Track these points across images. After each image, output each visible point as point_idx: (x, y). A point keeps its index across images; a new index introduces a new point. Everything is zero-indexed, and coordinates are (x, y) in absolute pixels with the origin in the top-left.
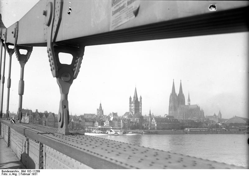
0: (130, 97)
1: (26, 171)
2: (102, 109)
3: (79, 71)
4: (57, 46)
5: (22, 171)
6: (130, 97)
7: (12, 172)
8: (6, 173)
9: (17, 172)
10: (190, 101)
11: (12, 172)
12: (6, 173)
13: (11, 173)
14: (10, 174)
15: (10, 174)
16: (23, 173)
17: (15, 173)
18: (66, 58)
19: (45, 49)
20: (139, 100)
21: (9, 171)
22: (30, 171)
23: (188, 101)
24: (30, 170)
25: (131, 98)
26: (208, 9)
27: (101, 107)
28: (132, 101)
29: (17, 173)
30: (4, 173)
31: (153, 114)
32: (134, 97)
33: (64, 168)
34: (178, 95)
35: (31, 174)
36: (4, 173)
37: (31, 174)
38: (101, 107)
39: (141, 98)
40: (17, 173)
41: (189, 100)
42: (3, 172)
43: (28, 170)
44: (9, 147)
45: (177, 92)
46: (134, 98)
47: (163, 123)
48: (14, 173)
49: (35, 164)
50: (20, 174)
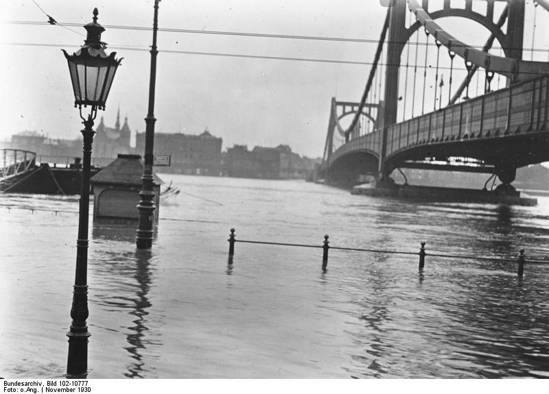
1: (58, 383)
4: (509, 19)
5: (48, 383)
7: (27, 384)
8: (13, 387)
9: (37, 385)
11: (27, 384)
12: (13, 387)
13: (25, 388)
14: (22, 390)
15: (22, 390)
16: (8, 387)
17: (33, 387)
18: (490, 74)
19: (91, 21)
21: (19, 384)
22: (66, 383)
24: (77, 380)
26: (158, 19)
29: (39, 388)
30: (10, 387)
33: (525, 374)
35: (77, 390)
36: (10, 387)
37: (77, 390)
40: (39, 388)
42: (7, 386)
43: (74, 380)
48: (31, 387)
50: (44, 389)
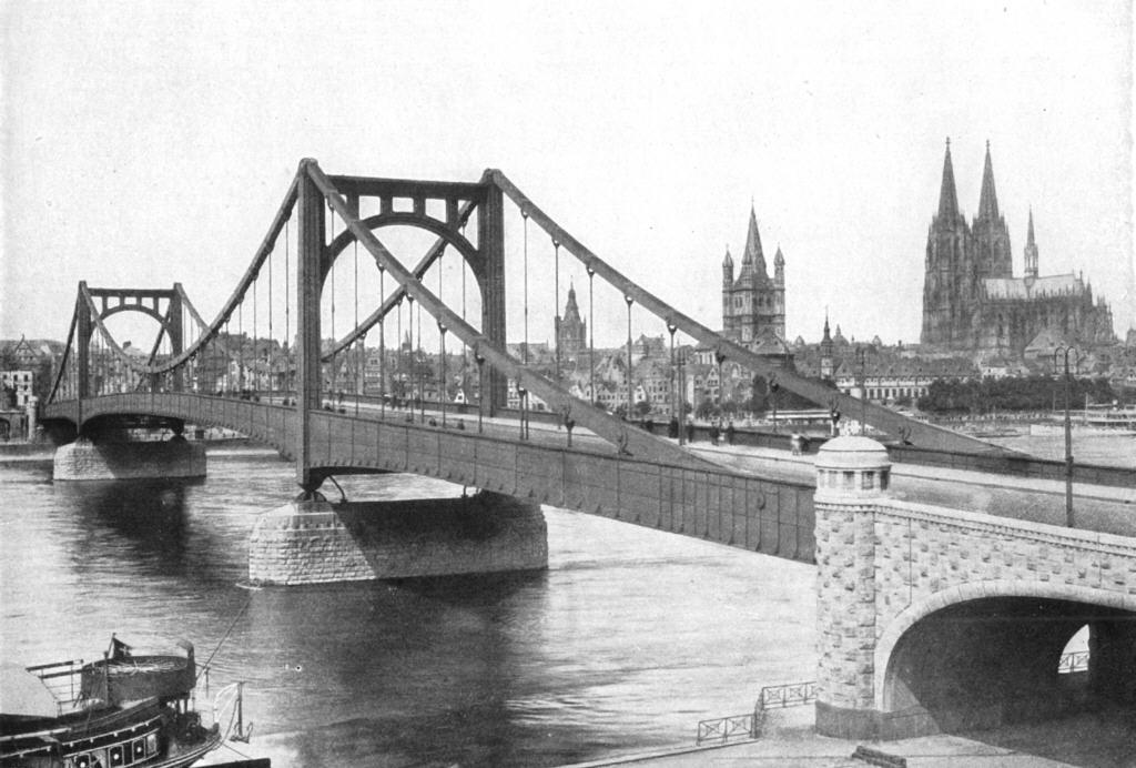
0: (779, 251)
2: (578, 317)
3: (243, 297)
6: (779, 251)
10: (1035, 254)
20: (771, 272)
23: (1027, 257)
25: (728, 268)
27: (573, 306)
28: (736, 276)
31: (838, 329)
32: (747, 262)
34: (971, 225)
38: (573, 306)
39: (780, 263)
41: (1032, 250)
44: (888, 491)
45: (969, 208)
46: (745, 263)
47: (894, 383)
49: (1090, 645)
